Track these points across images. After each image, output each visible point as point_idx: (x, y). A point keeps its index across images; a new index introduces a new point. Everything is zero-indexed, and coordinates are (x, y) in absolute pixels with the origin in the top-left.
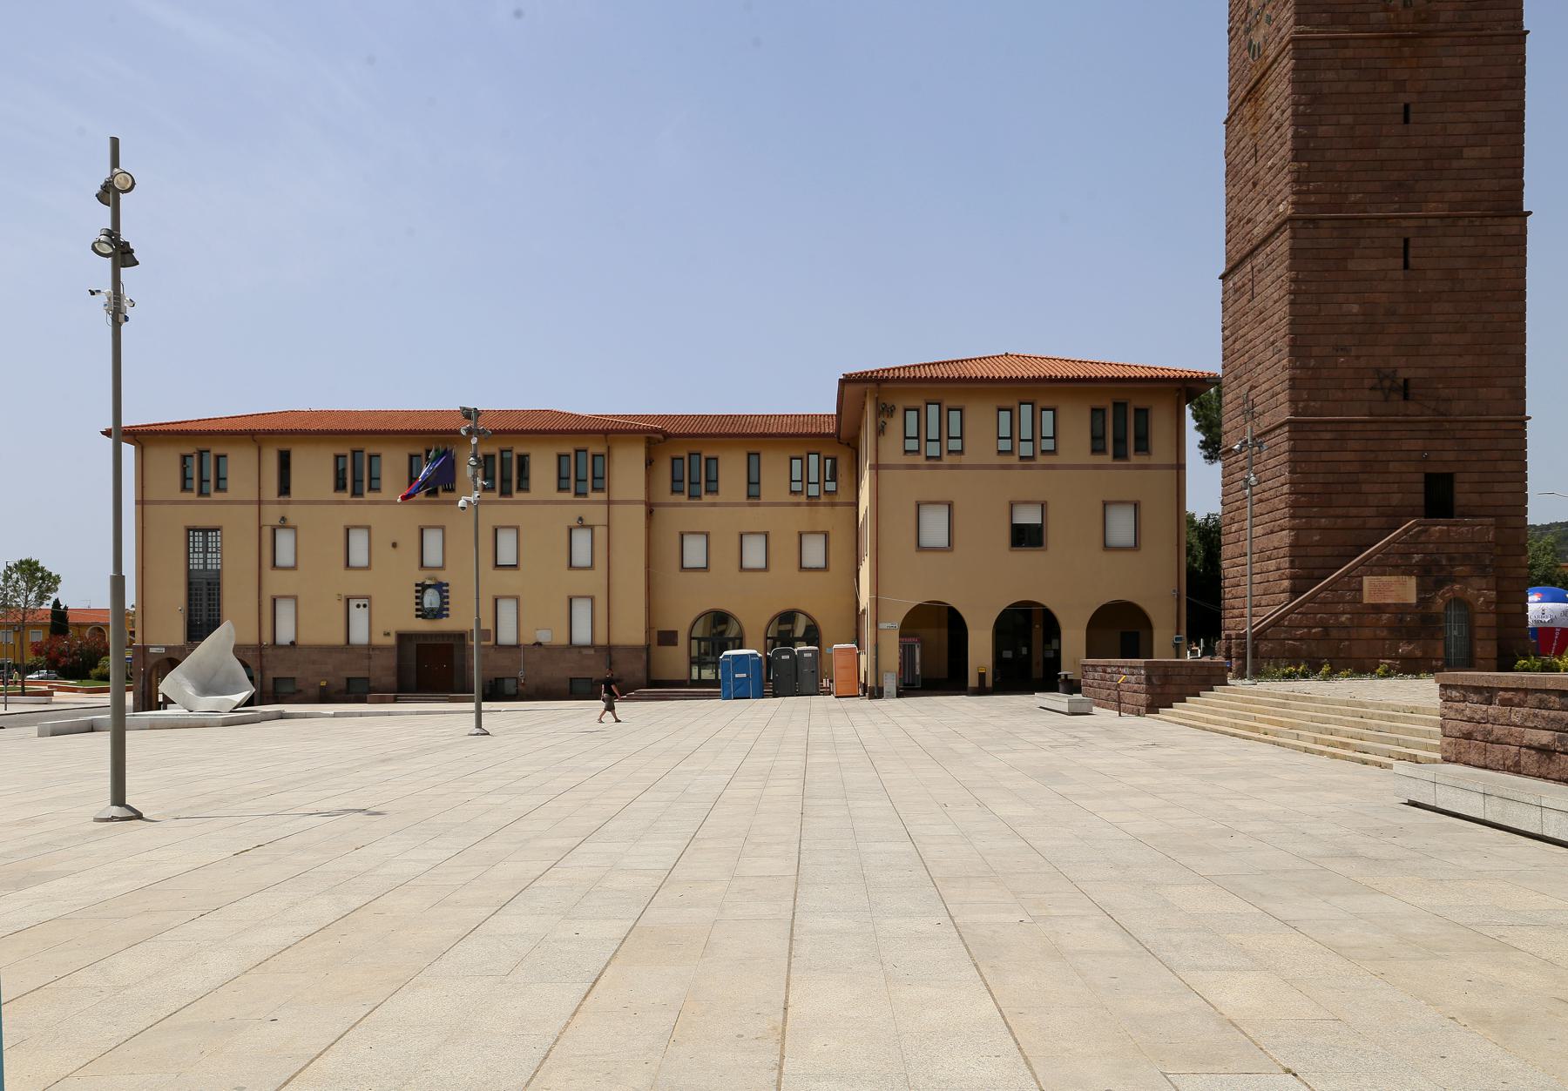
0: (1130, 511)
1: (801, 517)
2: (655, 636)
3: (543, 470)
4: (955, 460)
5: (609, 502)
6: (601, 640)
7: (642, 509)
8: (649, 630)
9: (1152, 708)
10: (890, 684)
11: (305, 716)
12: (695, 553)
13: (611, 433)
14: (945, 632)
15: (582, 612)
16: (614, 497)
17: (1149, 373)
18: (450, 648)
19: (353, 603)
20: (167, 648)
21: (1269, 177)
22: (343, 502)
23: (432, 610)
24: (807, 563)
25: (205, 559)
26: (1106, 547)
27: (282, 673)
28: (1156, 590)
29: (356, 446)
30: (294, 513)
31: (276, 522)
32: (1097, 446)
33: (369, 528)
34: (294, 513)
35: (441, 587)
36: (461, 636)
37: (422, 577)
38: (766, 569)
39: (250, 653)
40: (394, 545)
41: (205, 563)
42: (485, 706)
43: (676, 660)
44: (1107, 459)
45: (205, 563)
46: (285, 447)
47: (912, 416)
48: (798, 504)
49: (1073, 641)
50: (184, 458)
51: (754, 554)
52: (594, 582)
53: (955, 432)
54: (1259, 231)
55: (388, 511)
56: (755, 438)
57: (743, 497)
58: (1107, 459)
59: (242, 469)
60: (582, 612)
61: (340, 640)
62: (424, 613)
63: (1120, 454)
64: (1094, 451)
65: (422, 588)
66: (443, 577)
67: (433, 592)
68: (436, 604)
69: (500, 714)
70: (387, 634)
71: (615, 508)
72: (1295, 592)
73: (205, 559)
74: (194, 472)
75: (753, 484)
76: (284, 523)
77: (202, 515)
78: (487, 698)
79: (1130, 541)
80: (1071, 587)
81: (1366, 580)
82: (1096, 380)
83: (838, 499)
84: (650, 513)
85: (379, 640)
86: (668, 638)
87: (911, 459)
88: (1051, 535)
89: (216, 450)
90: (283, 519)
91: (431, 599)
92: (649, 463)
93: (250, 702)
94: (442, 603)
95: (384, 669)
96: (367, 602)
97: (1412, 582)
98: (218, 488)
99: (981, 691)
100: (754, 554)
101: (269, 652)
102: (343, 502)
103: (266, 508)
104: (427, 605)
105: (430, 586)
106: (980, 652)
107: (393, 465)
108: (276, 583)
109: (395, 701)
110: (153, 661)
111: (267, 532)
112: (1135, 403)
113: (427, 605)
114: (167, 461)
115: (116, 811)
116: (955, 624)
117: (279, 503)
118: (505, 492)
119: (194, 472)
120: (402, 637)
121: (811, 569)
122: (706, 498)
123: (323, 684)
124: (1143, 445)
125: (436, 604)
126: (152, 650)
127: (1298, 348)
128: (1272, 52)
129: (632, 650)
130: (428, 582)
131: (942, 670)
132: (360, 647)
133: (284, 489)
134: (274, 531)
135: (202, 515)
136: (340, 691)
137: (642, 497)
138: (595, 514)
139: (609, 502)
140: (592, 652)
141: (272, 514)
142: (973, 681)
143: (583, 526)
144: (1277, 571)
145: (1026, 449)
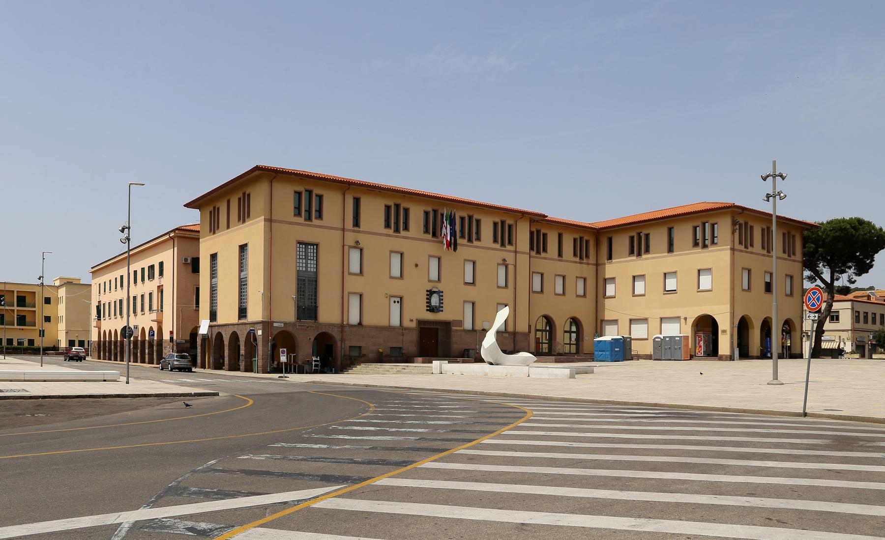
6: (510, 329)
20: (285, 324)
23: (436, 307)
25: (306, 264)
27: (355, 343)
30: (361, 237)
31: (353, 244)
35: (440, 293)
36: (447, 325)
39: (336, 329)
40: (417, 265)
41: (306, 267)
42: (781, 362)
45: (306, 267)
46: (357, 195)
50: (695, 228)
52: (353, 284)
55: (416, 243)
59: (334, 206)
63: (397, 230)
70: (411, 321)
73: (306, 264)
74: (699, 236)
76: (356, 245)
77: (309, 233)
78: (781, 357)
85: (407, 324)
88: (678, 291)
90: (357, 242)
91: (435, 301)
95: (410, 343)
101: (347, 329)
102: (389, 236)
107: (417, 216)
108: (353, 284)
110: (275, 332)
112: (509, 221)
117: (354, 231)
119: (699, 236)
120: (420, 322)
126: (275, 325)
130: (435, 290)
133: (356, 223)
135: (309, 233)
136: (387, 356)
139: (516, 252)
140: (506, 335)
141: (350, 238)
143: (503, 264)
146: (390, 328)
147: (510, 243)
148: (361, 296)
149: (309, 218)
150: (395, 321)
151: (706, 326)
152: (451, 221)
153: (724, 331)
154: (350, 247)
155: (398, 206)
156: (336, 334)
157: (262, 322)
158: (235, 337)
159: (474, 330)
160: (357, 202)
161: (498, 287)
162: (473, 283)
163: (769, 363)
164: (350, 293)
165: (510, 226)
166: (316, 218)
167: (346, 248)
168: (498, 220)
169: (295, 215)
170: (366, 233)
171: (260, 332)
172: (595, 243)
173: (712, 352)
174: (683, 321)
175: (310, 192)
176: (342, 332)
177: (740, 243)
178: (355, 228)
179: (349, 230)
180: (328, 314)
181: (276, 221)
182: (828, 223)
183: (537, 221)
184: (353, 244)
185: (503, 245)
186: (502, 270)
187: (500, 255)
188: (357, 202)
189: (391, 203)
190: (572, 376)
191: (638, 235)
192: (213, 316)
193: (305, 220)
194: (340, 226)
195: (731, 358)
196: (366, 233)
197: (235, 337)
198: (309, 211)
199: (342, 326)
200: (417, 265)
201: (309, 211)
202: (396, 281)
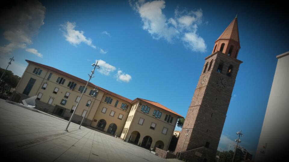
0: (167, 129)
1: (121, 112)
2: (94, 120)
4: (147, 114)
5: (95, 99)
6: (86, 117)
7: (100, 102)
8: (93, 119)
10: (128, 140)
11: (55, 118)
12: (104, 110)
13: (100, 90)
14: (136, 136)
15: (85, 112)
16: (97, 99)
18: (63, 110)
19: (51, 98)
21: (199, 99)
26: (162, 133)
28: (167, 141)
29: (63, 77)
30: (48, 82)
32: (165, 120)
33: (162, 133)
34: (48, 82)
36: (65, 109)
38: (113, 116)
42: (81, 126)
43: (95, 124)
44: (166, 122)
47: (143, 106)
49: (153, 144)
51: (112, 114)
53: (148, 110)
54: (196, 104)
56: (119, 98)
57: (114, 106)
58: (166, 122)
60: (85, 112)
61: (47, 102)
62: (61, 104)
63: (168, 122)
66: (67, 99)
67: (64, 102)
68: (64, 103)
70: (54, 104)
71: (96, 100)
72: (187, 150)
76: (46, 83)
78: (73, 121)
79: (141, 124)
80: (156, 136)
81: (196, 152)
83: (127, 111)
84: (100, 103)
85: (53, 105)
86: (95, 121)
87: (141, 112)
88: (57, 93)
89: (41, 69)
91: (64, 102)
92: (103, 96)
93: (34, 108)
96: (53, 99)
97: (201, 154)
98: (39, 74)
99: (139, 146)
100: (112, 114)
103: (45, 80)
106: (141, 140)
109: (52, 115)
111: (43, 83)
112: (172, 116)
114: (33, 68)
116: (138, 135)
118: (108, 103)
120: (57, 106)
122: (109, 104)
123: (41, 108)
124: (171, 122)
125: (64, 103)
126: (17, 93)
127: (196, 121)
128: (204, 85)
129: (90, 120)
131: (134, 140)
133: (48, 79)
134: (44, 84)
135: (34, 77)
137: (100, 100)
139: (95, 99)
141: (45, 81)
142: (138, 144)
144: (186, 146)
145: (156, 116)
146: (48, 104)
159: (81, 116)
161: (118, 118)
163: (80, 125)
167: (43, 83)
168: (72, 81)
170: (51, 82)
181: (45, 78)
196: (51, 82)
201: (168, 120)
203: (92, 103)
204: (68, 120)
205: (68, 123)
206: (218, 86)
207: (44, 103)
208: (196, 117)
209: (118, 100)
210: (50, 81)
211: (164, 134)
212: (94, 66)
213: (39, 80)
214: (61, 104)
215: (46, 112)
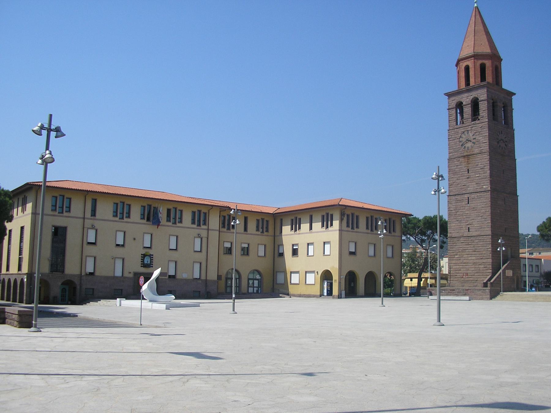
3: (187, 217)
9: (491, 299)
10: (343, 295)
17: (385, 210)
22: (116, 221)
24: (260, 255)
30: (97, 224)
35: (151, 256)
37: (144, 252)
40: (134, 239)
42: (236, 300)
48: (258, 235)
60: (197, 266)
64: (192, 223)
65: (144, 256)
66: (151, 252)
69: (243, 304)
70: (130, 273)
75: (311, 228)
76: (93, 227)
79: (391, 256)
82: (371, 209)
85: (126, 275)
91: (147, 260)
94: (151, 262)
102: (116, 221)
104: (146, 262)
105: (147, 255)
113: (146, 262)
115: (438, 323)
117: (91, 219)
121: (121, 258)
132: (117, 277)
133: (94, 213)
135: (60, 221)
138: (204, 234)
143: (199, 237)
146: (115, 277)
147: (205, 224)
148: (176, 262)
149: (175, 223)
150: (118, 273)
151: (327, 276)
152: (154, 211)
153: (335, 280)
154: (88, 228)
155: (122, 204)
156: (77, 281)
157: (27, 274)
158: (15, 281)
160: (94, 202)
162: (123, 246)
163: (381, 299)
164: (86, 256)
165: (205, 214)
166: (126, 217)
167: (85, 229)
169: (141, 219)
171: (25, 280)
172: (270, 223)
173: (330, 293)
174: (316, 274)
175: (176, 209)
176: (81, 280)
177: (348, 226)
178: (92, 217)
179: (88, 219)
180: (71, 268)
181: (211, 230)
182: (547, 219)
183: (224, 210)
184: (90, 226)
185: (199, 225)
186: (198, 241)
187: (198, 231)
188: (94, 202)
189: (259, 218)
190: (167, 308)
191: (295, 218)
192: (8, 269)
193: (173, 223)
194: (81, 215)
195: (340, 297)
197: (15, 281)
198: (199, 221)
199: (81, 275)
200: (134, 239)
201: (199, 221)
202: (198, 253)
203: (204, 240)
204: (380, 297)
205: (435, 304)
206: (500, 146)
207: (107, 278)
208: (489, 213)
209: (246, 216)
210: (162, 225)
211: (372, 256)
212: (45, 133)
213: (72, 224)
214: (144, 267)
215: (209, 296)
